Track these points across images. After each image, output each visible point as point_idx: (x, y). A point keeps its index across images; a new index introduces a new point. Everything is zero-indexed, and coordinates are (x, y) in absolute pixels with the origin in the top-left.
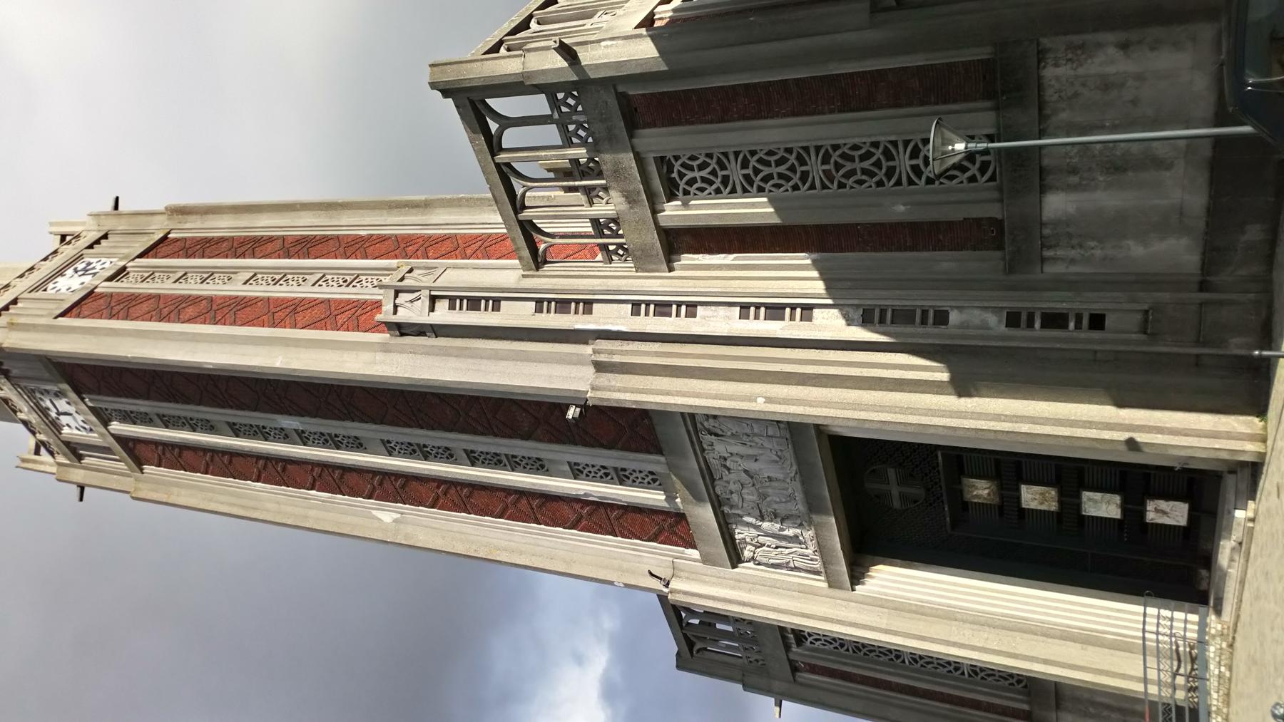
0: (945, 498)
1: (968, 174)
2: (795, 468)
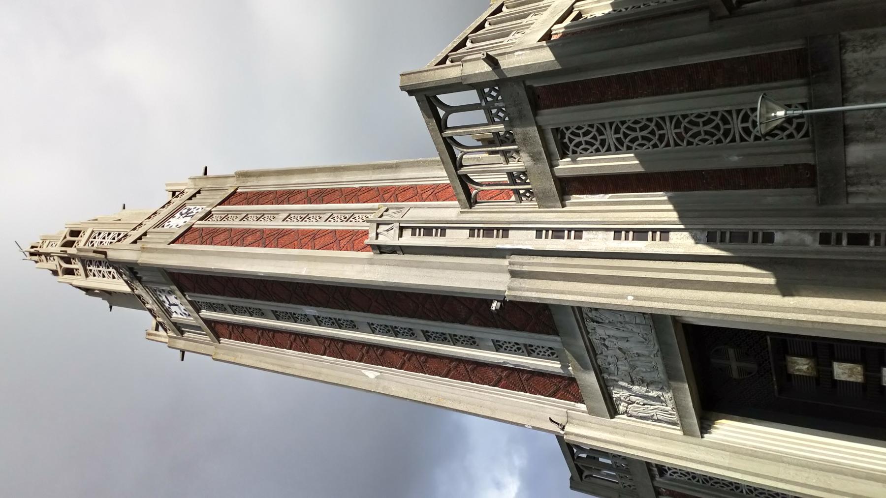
2: (657, 347)
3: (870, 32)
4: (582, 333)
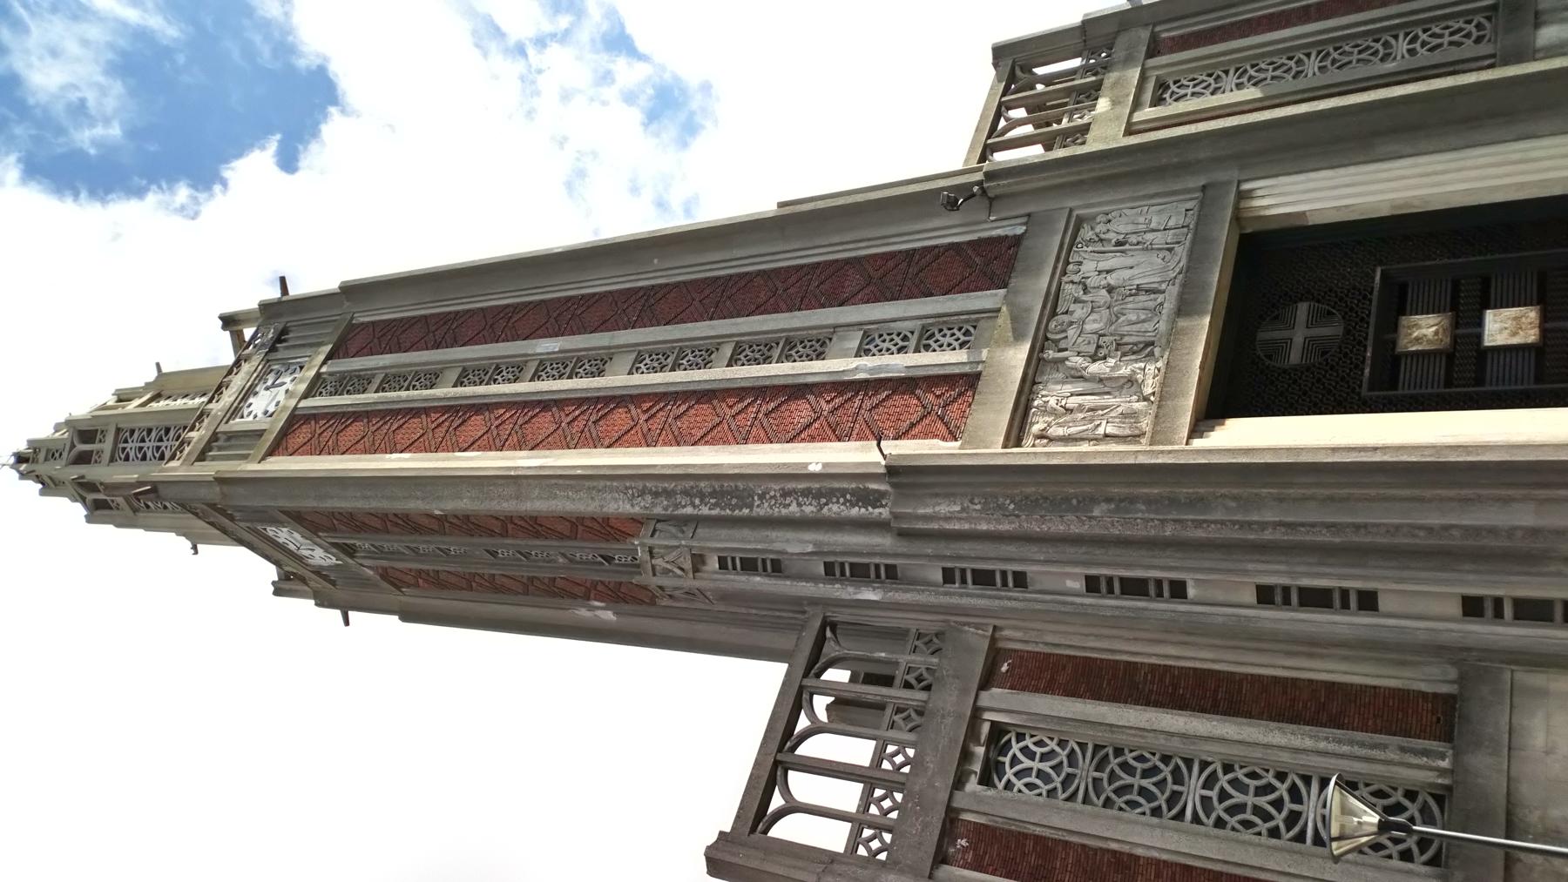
1: (1271, 824)
4: (1055, 268)
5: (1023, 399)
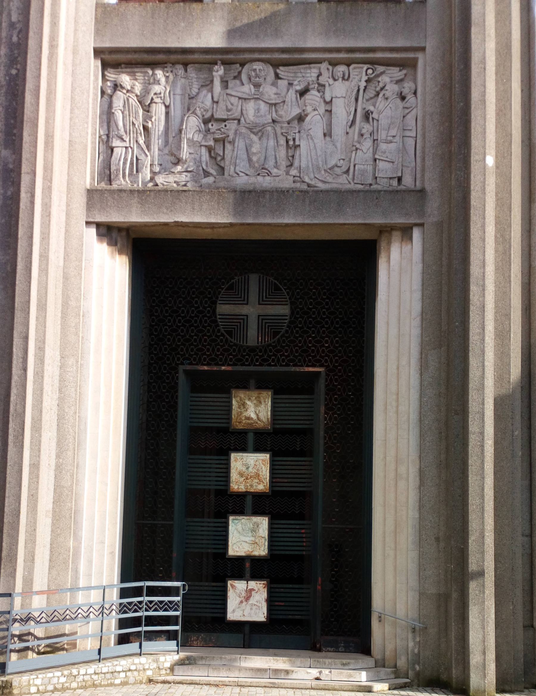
0: (241, 368)
2: (322, 186)
3: (344, 661)
4: (338, 50)
5: (161, 57)
